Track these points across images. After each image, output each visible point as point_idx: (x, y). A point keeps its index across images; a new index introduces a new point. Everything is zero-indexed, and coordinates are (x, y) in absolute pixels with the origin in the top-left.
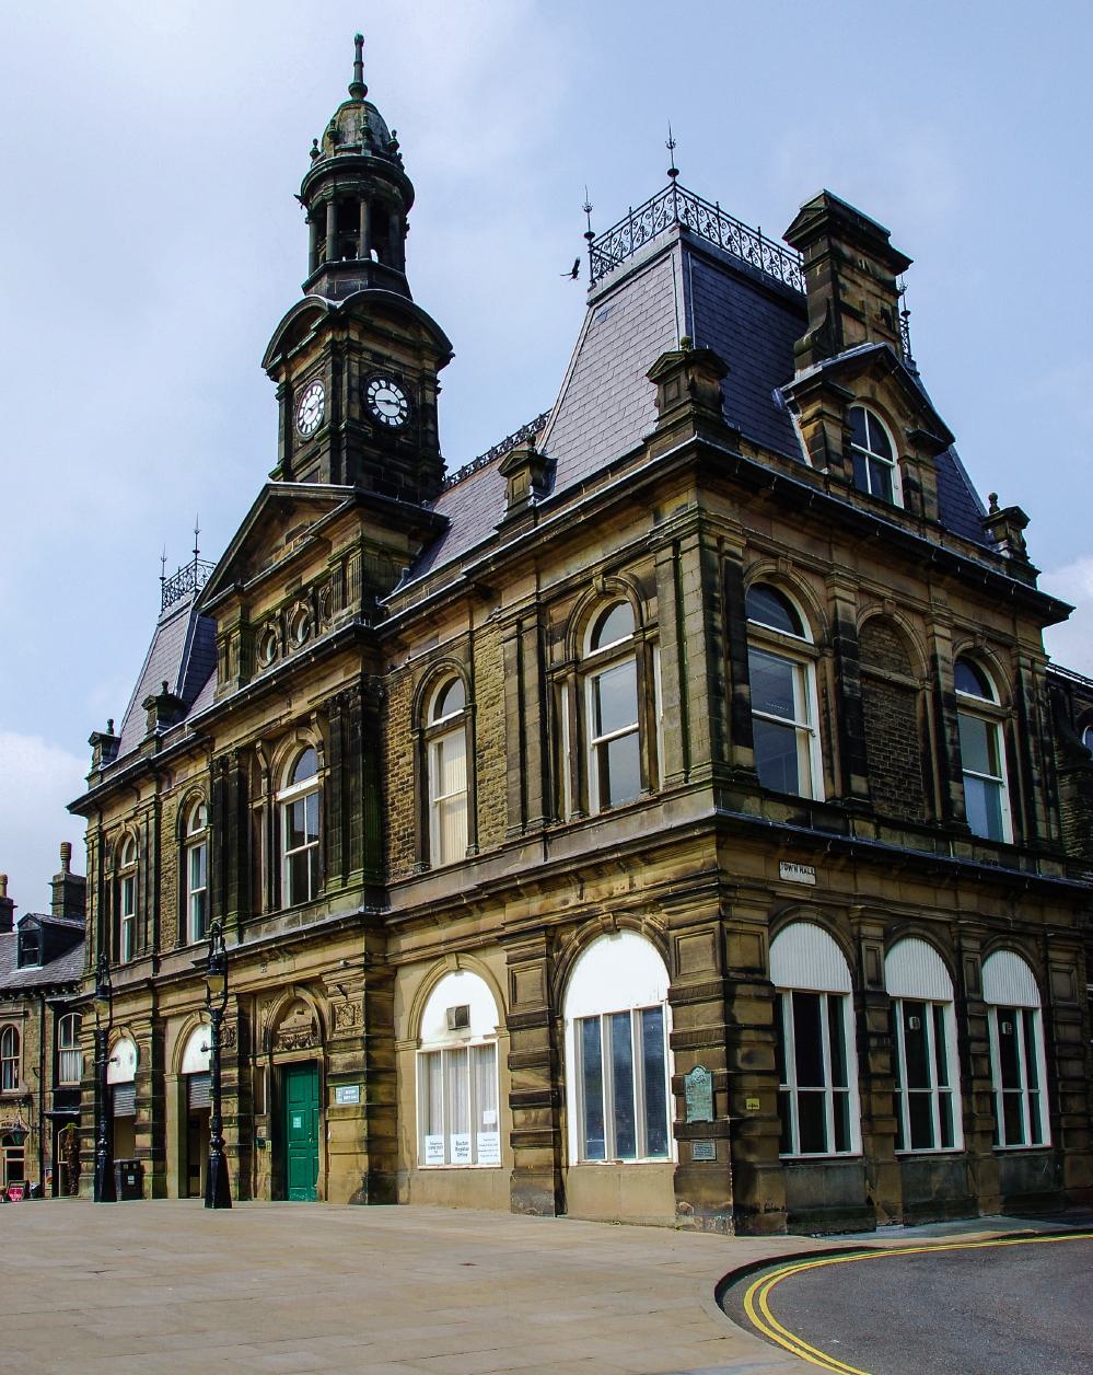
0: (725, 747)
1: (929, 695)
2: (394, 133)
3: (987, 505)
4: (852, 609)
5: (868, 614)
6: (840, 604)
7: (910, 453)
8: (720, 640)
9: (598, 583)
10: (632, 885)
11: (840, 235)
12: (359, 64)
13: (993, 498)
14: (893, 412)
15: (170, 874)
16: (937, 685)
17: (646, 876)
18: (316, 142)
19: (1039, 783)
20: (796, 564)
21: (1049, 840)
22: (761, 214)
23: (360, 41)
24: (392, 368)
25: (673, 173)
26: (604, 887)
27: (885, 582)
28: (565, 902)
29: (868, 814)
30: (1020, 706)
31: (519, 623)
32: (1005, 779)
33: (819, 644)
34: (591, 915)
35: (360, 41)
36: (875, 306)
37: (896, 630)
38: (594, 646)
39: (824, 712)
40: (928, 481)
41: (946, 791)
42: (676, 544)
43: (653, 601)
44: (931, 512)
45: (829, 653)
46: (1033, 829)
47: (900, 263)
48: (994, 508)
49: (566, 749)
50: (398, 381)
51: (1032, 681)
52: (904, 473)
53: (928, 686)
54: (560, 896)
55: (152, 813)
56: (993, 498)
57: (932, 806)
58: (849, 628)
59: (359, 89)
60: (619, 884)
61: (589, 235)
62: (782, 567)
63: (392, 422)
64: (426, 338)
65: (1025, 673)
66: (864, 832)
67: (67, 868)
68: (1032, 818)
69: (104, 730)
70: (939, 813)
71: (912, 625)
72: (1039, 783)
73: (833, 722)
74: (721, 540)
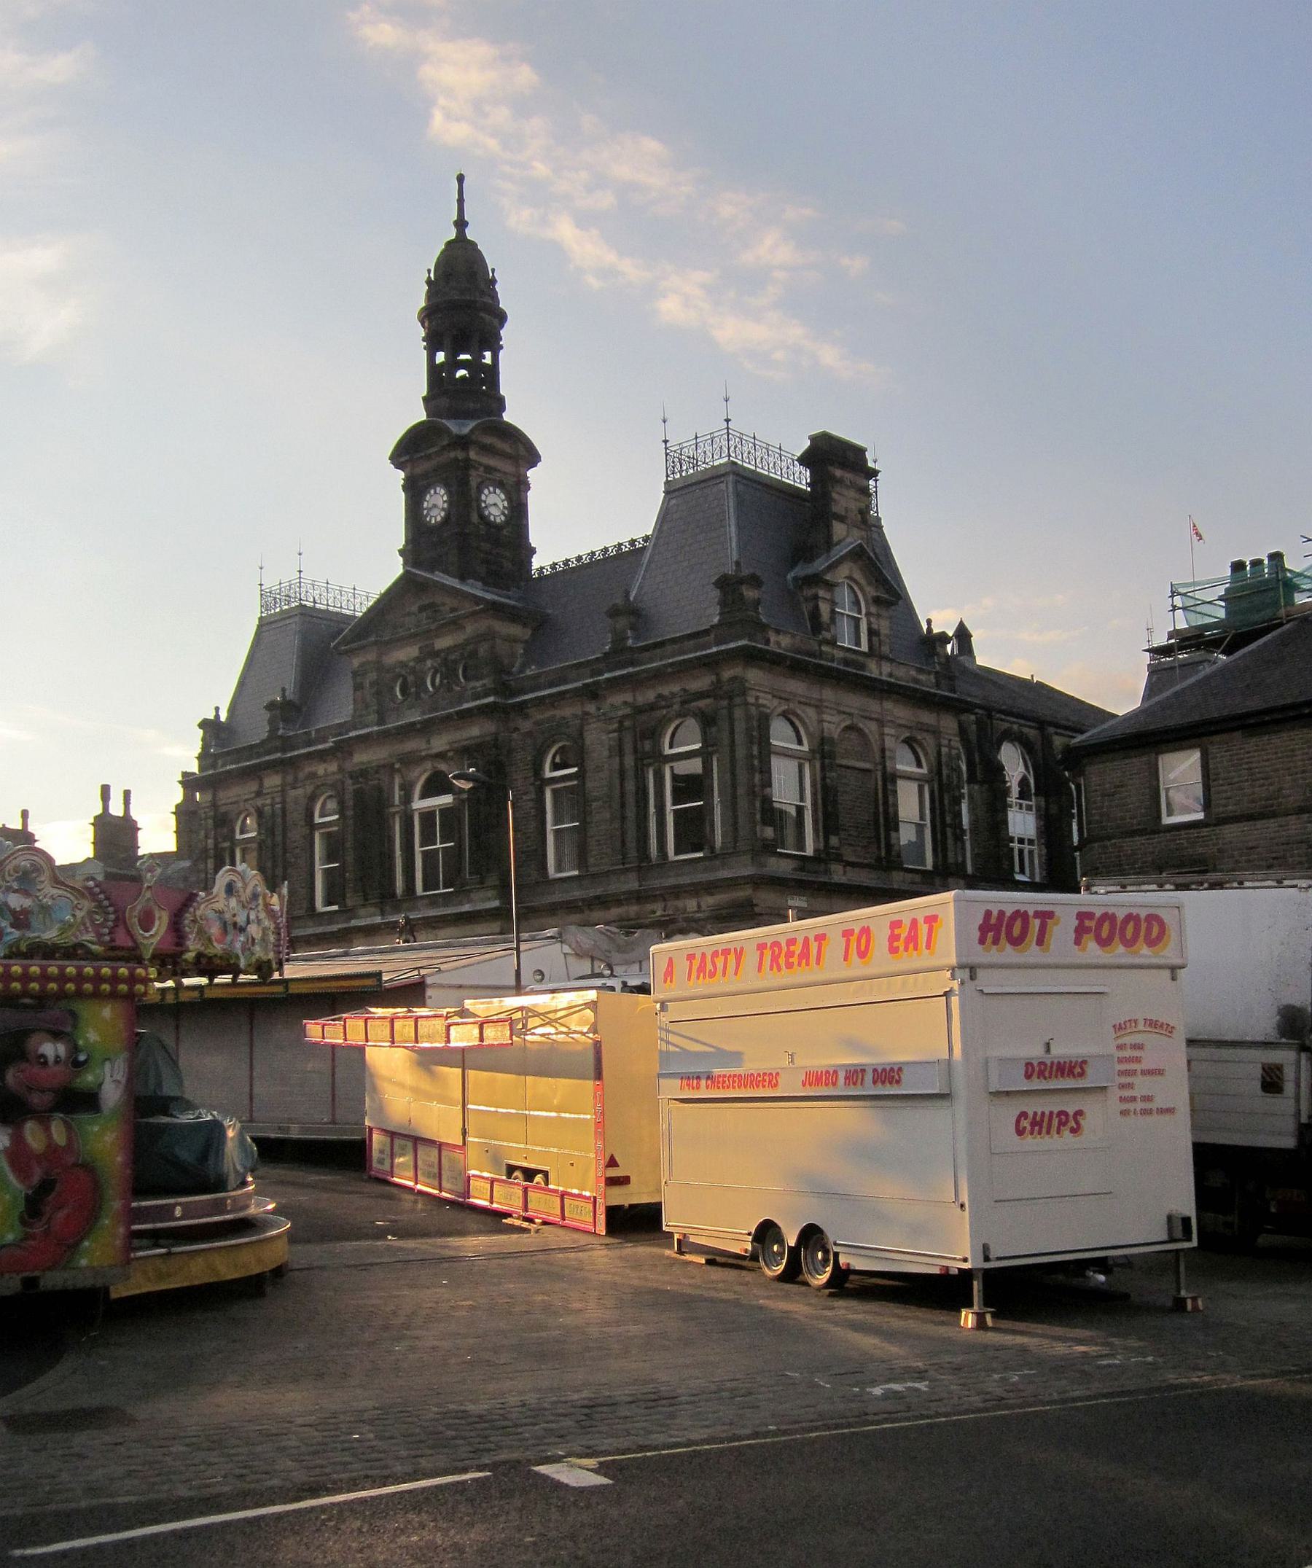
0: (758, 828)
1: (879, 774)
2: (493, 270)
3: (925, 627)
4: (833, 725)
5: (843, 725)
6: (825, 725)
7: (873, 609)
8: (756, 762)
9: (676, 707)
10: (699, 906)
11: (836, 461)
12: (461, 201)
13: (929, 622)
14: (863, 582)
15: (297, 851)
16: (885, 767)
17: (709, 901)
18: (429, 271)
19: (950, 826)
20: (800, 703)
21: (956, 864)
22: (783, 461)
23: (461, 179)
24: (497, 476)
25: (728, 421)
26: (680, 904)
27: (854, 701)
28: (654, 912)
29: (839, 859)
30: (939, 773)
31: (621, 723)
32: (928, 822)
33: (812, 751)
34: (673, 921)
35: (461, 179)
36: (853, 506)
37: (860, 731)
38: (671, 747)
39: (814, 794)
40: (884, 626)
41: (888, 838)
42: (731, 698)
43: (714, 729)
44: (885, 649)
45: (818, 756)
46: (945, 857)
47: (873, 474)
48: (930, 629)
49: (652, 810)
50: (501, 485)
51: (949, 755)
52: (869, 624)
53: (880, 767)
54: (649, 907)
55: (278, 800)
56: (929, 622)
57: (879, 848)
58: (831, 740)
59: (461, 224)
60: (691, 904)
61: (666, 442)
62: (792, 706)
63: (498, 520)
64: (522, 451)
65: (944, 750)
66: (839, 874)
67: (106, 807)
68: (945, 850)
69: (212, 717)
70: (883, 854)
71: (871, 728)
72: (950, 826)
73: (820, 802)
74: (757, 698)
